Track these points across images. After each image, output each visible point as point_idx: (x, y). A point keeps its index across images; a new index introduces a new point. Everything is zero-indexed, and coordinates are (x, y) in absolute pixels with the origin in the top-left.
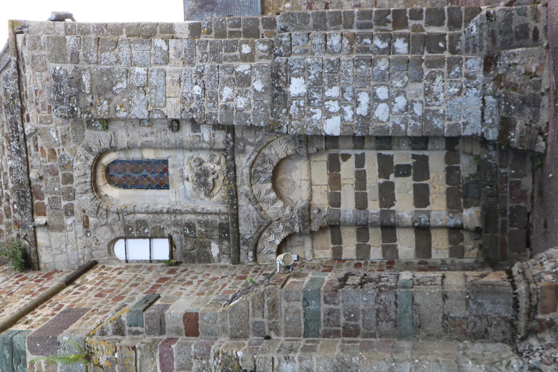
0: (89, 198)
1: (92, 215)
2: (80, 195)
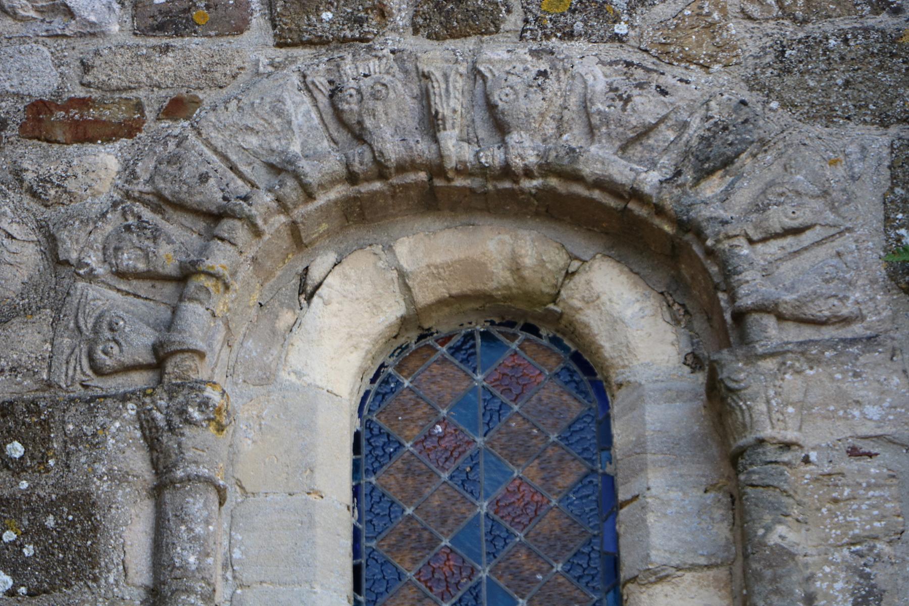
0: (296, 148)
1: (144, 169)
2: (321, 80)
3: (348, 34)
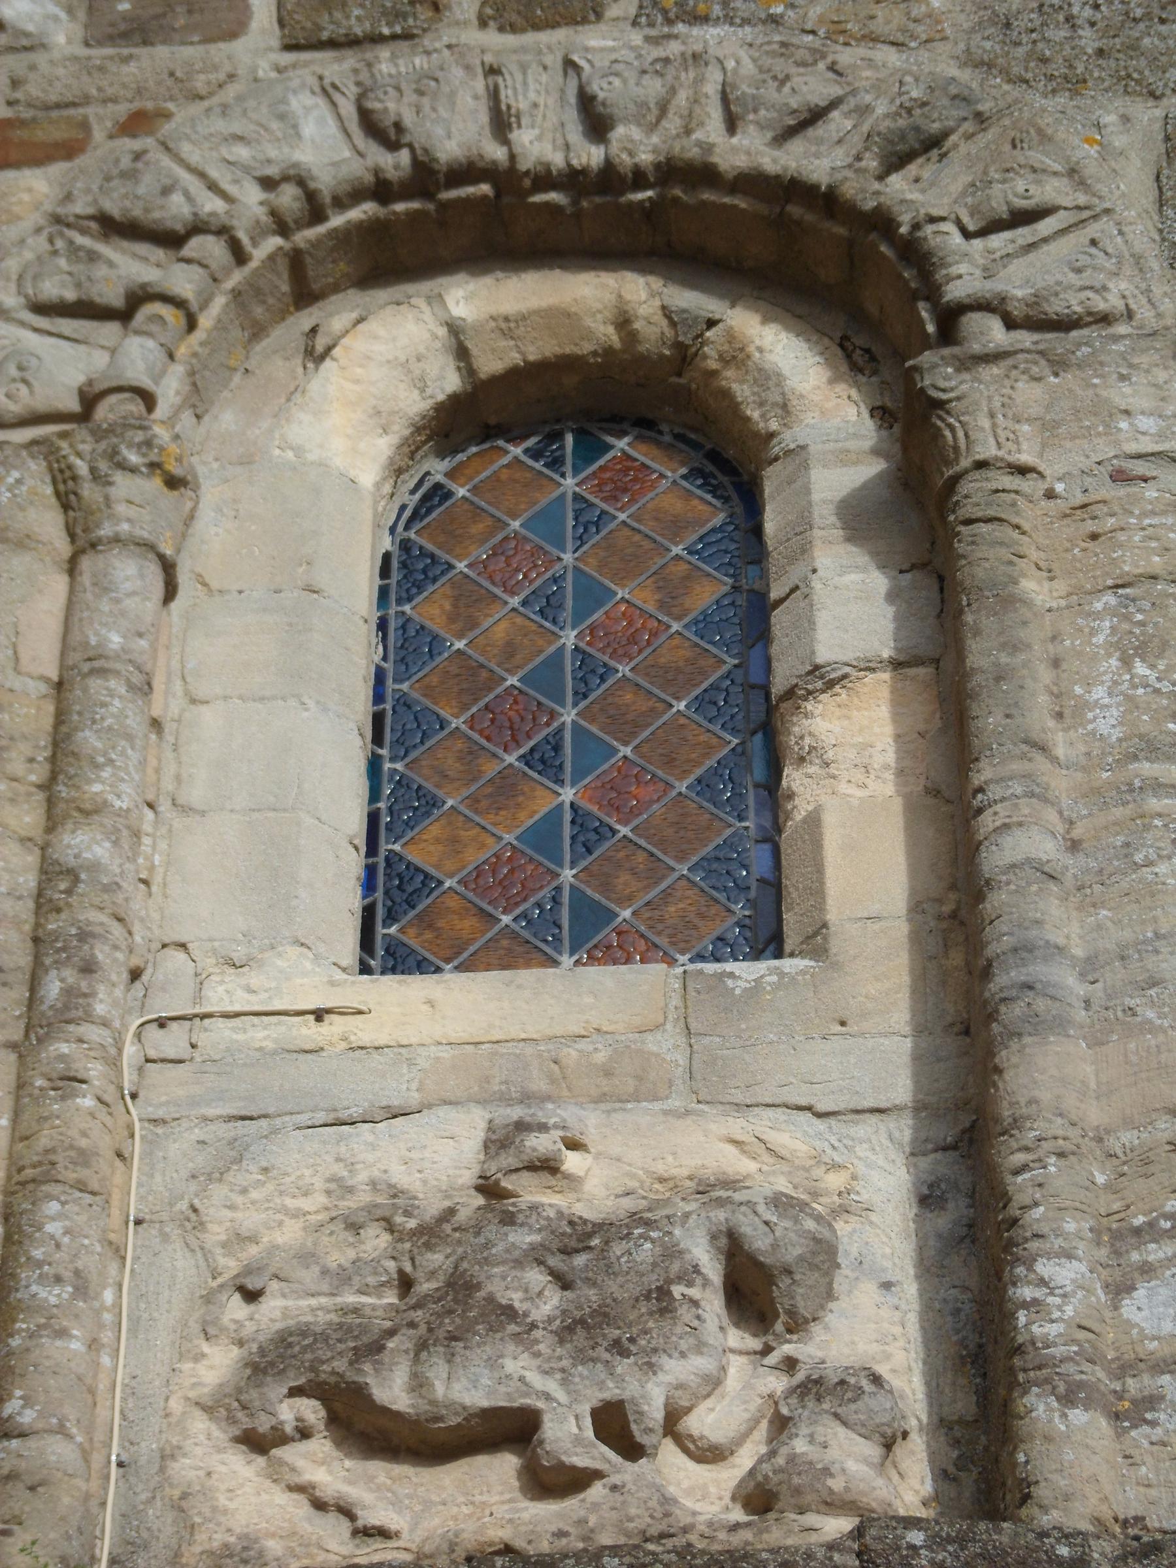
3: (386, 31)
